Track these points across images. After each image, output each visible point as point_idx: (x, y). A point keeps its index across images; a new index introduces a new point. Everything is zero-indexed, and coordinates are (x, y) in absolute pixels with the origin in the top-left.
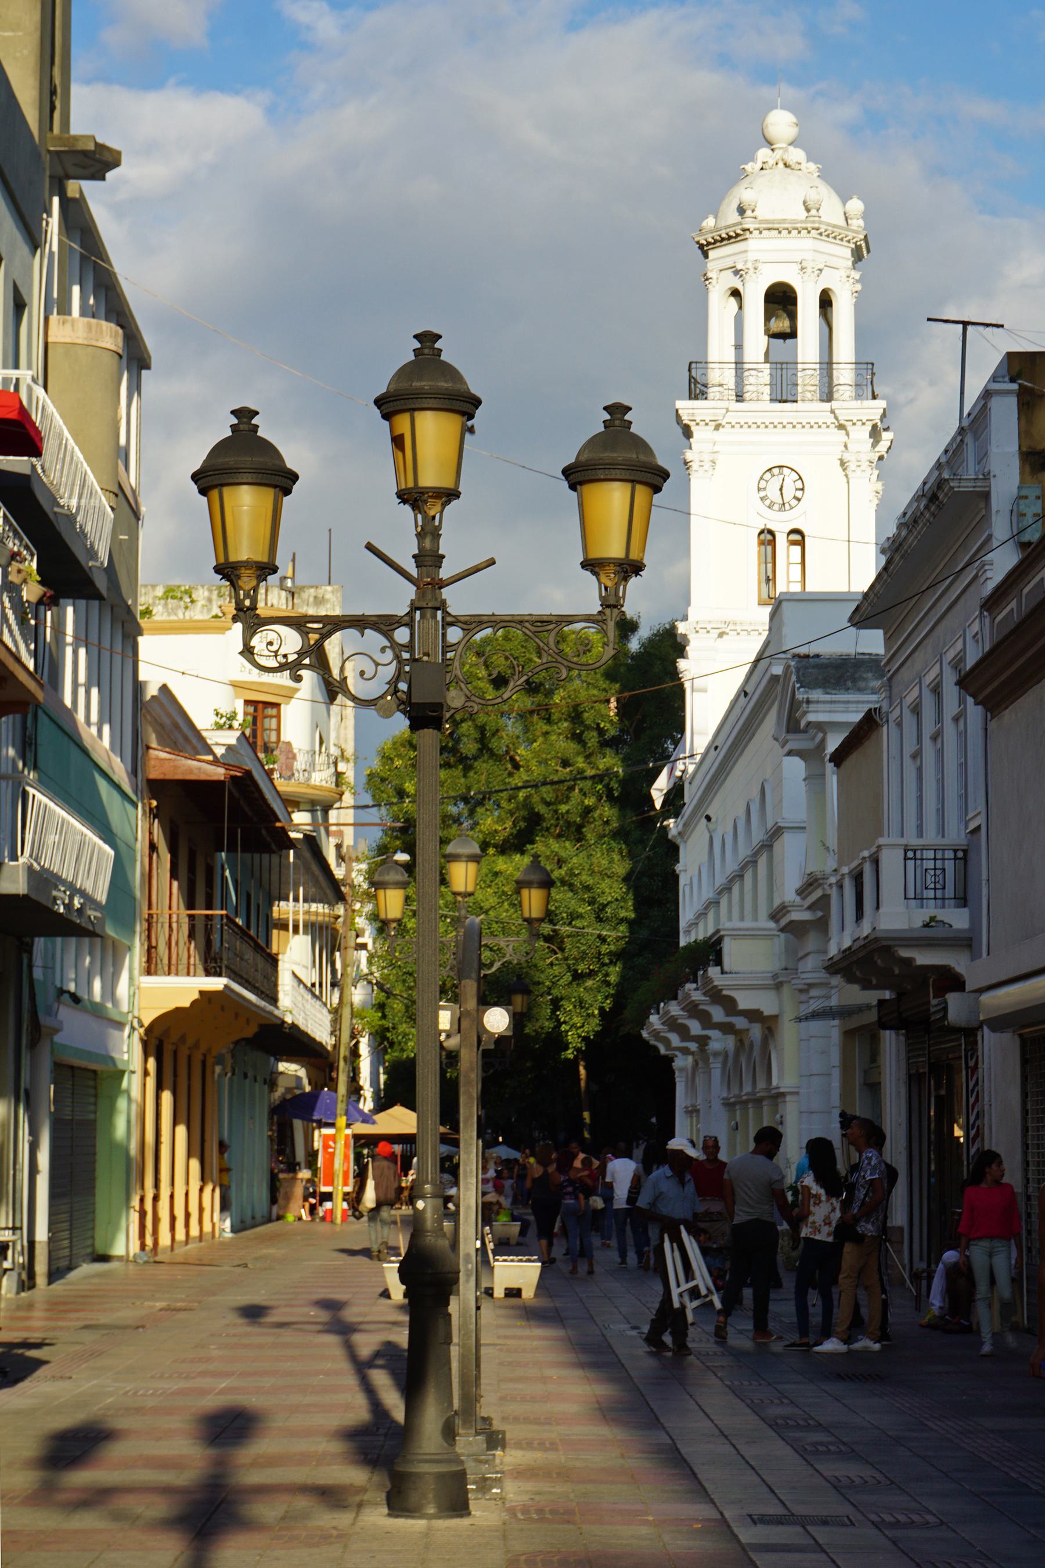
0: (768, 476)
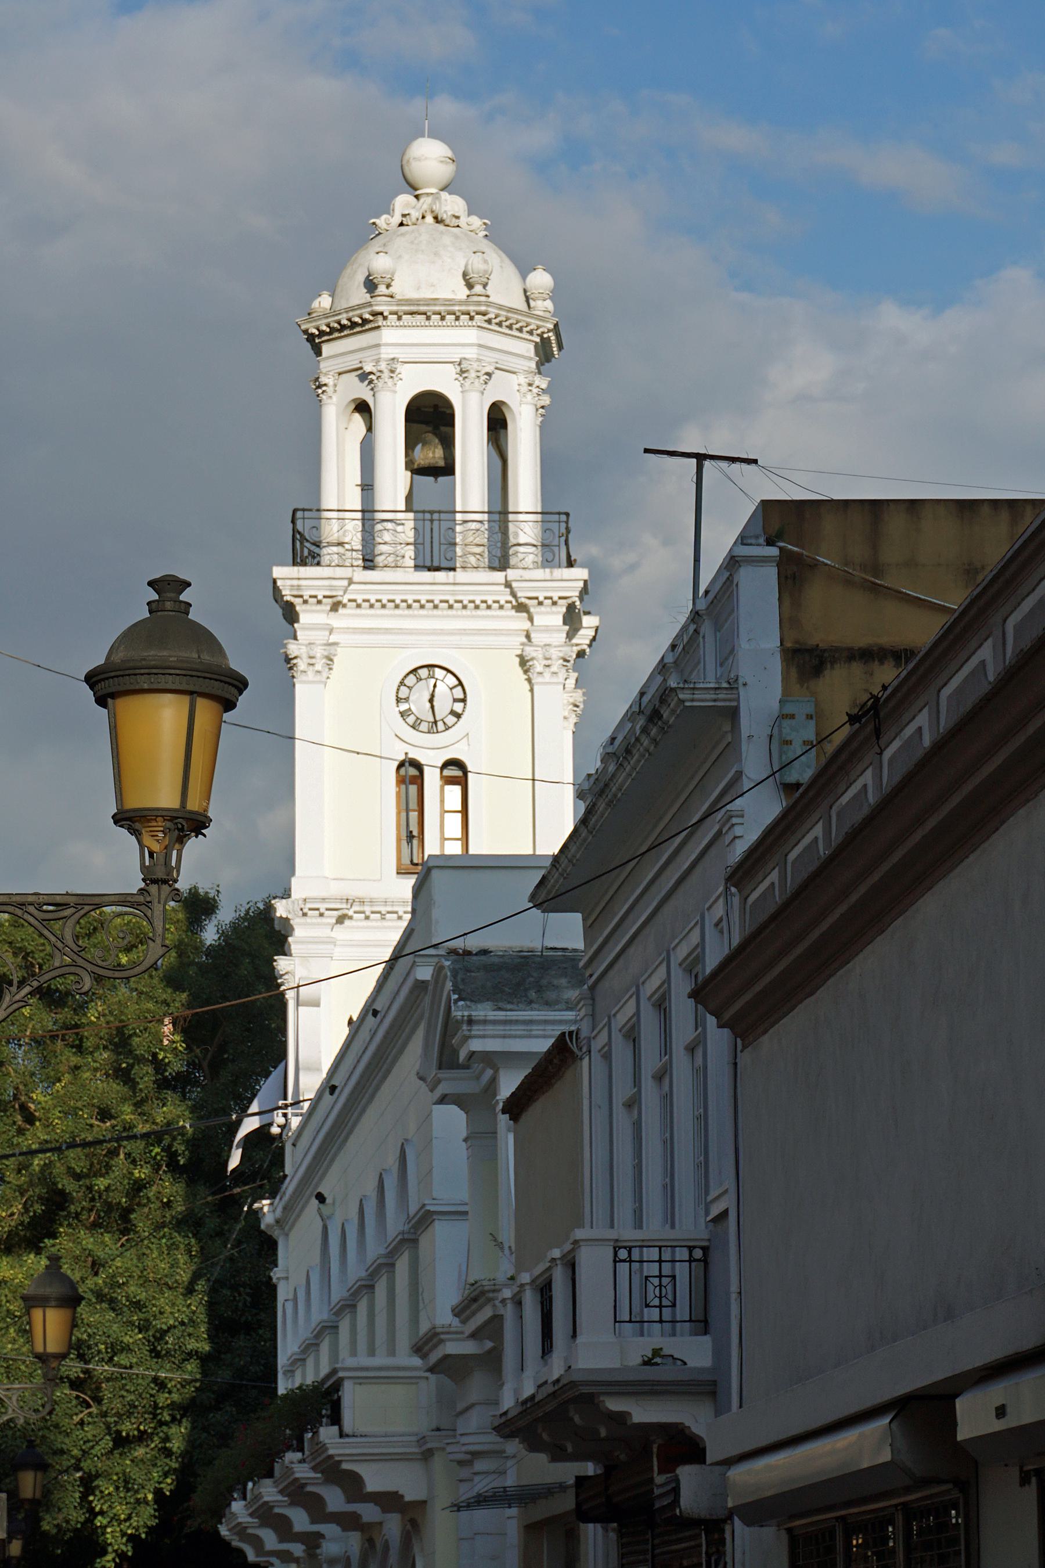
0: (411, 680)
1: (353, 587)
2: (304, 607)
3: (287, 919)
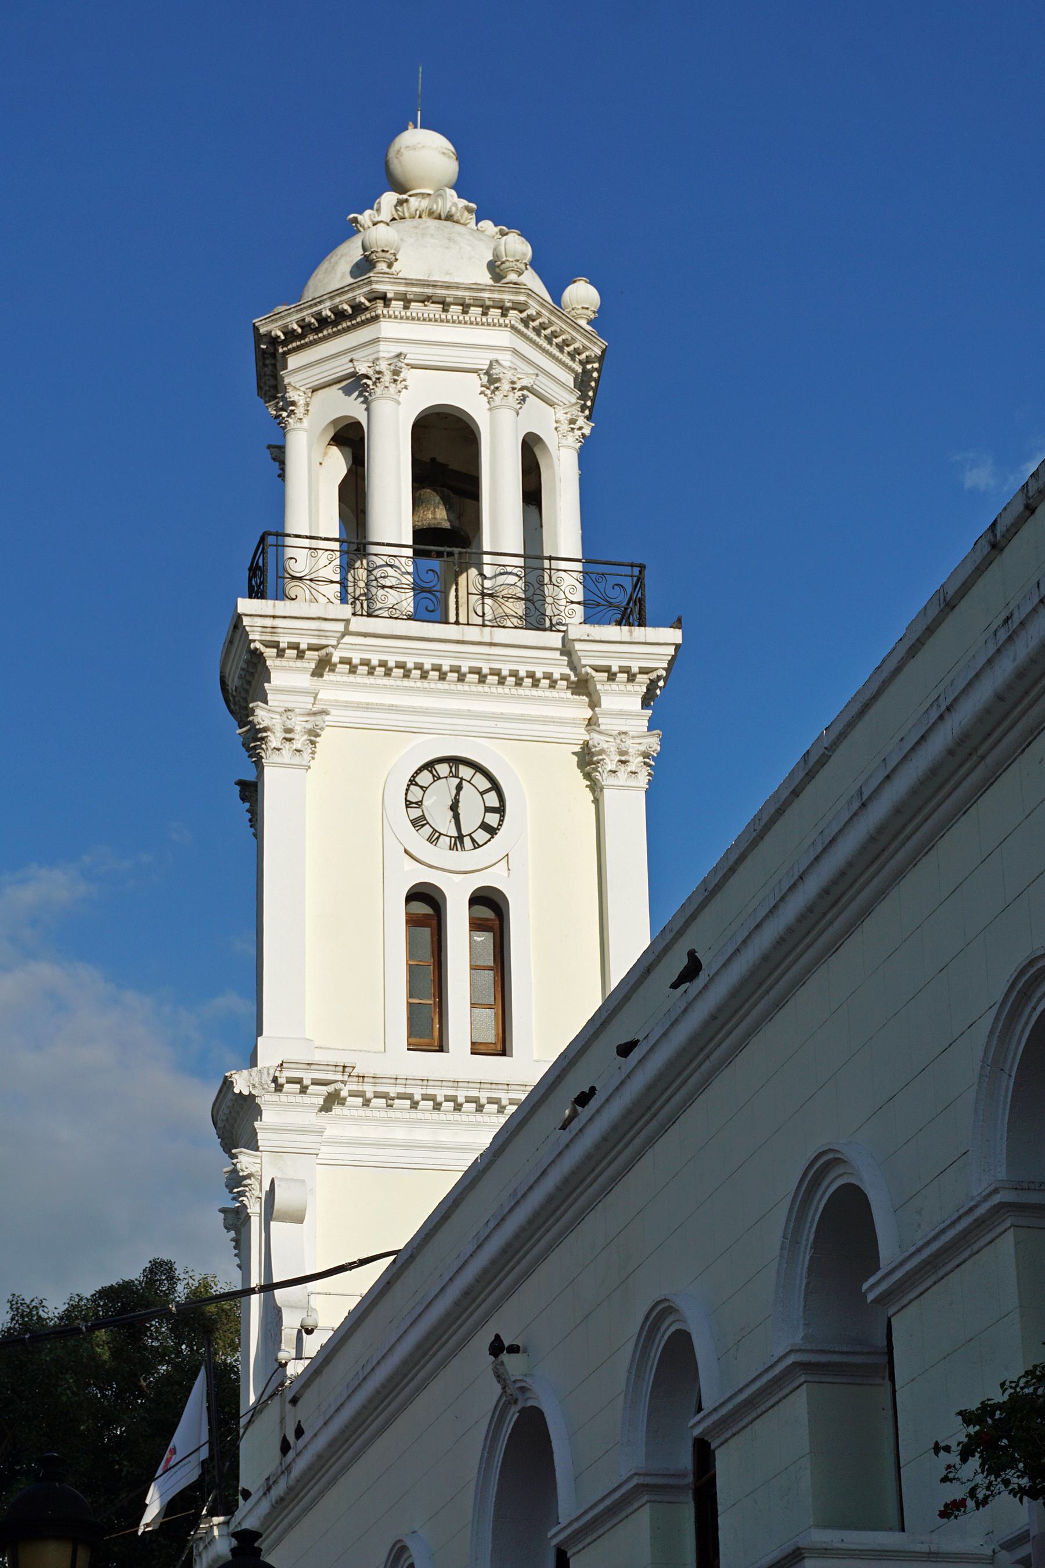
0: (425, 778)
1: (347, 639)
2: (278, 662)
3: (252, 1097)
